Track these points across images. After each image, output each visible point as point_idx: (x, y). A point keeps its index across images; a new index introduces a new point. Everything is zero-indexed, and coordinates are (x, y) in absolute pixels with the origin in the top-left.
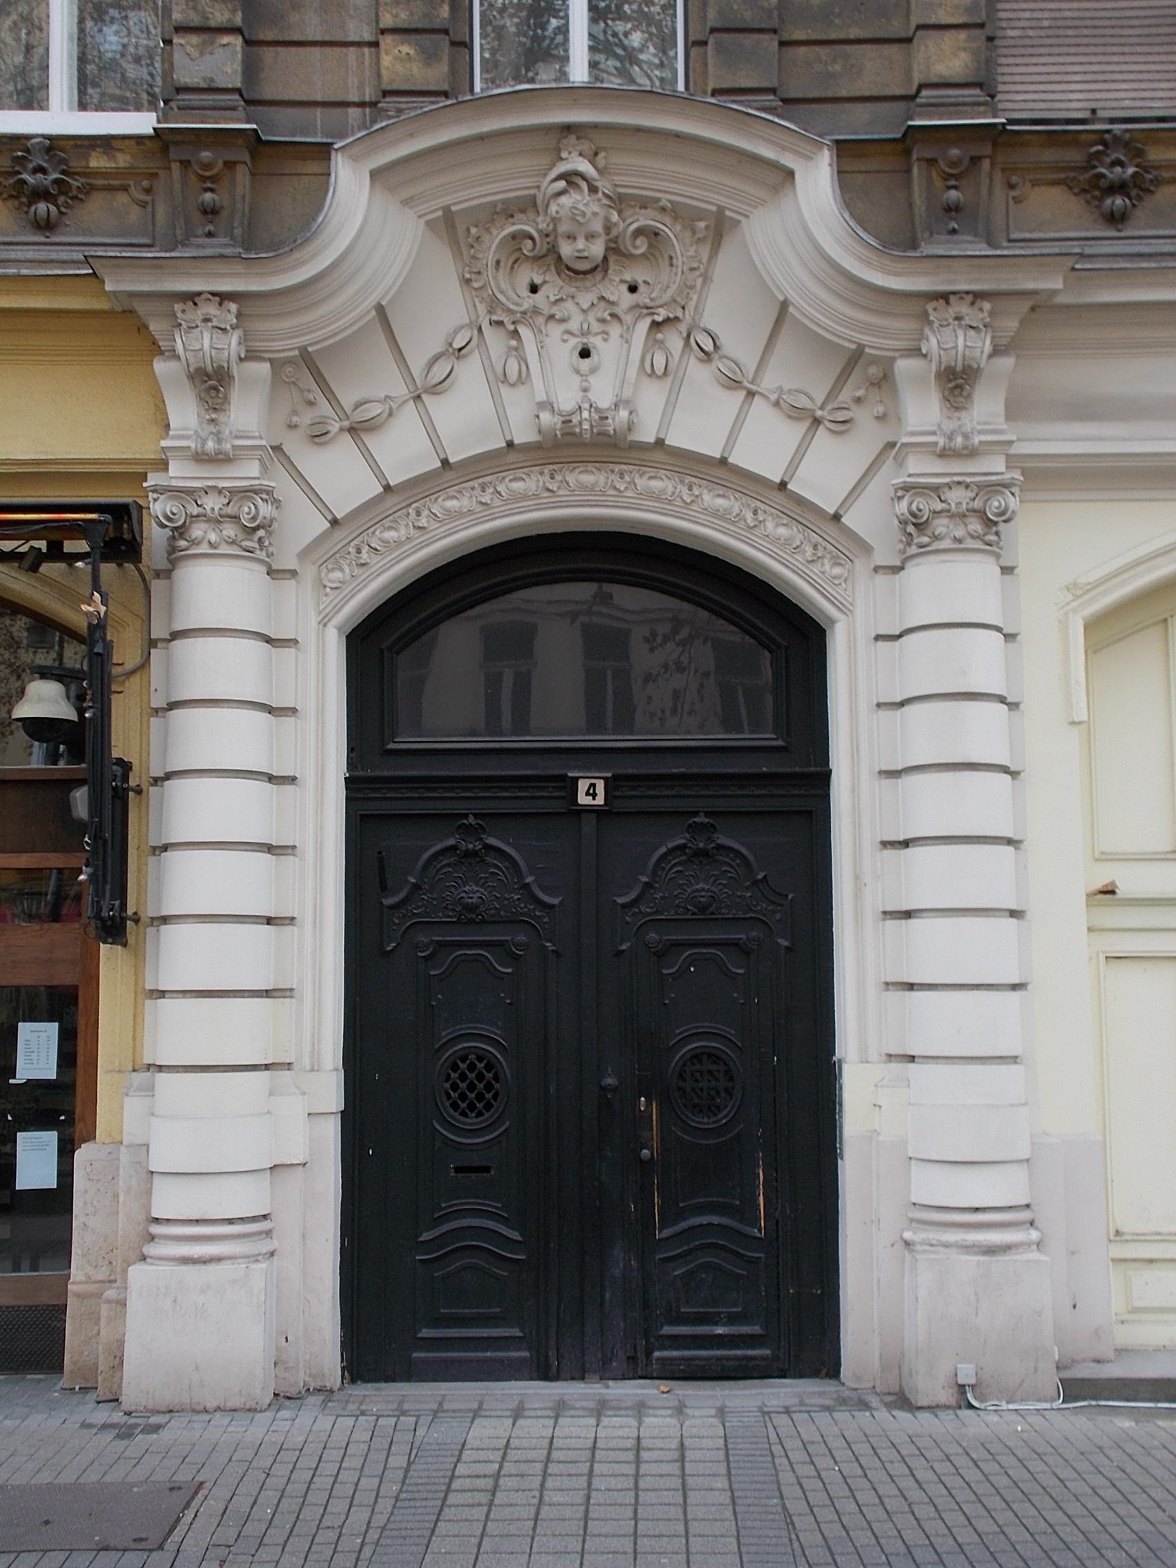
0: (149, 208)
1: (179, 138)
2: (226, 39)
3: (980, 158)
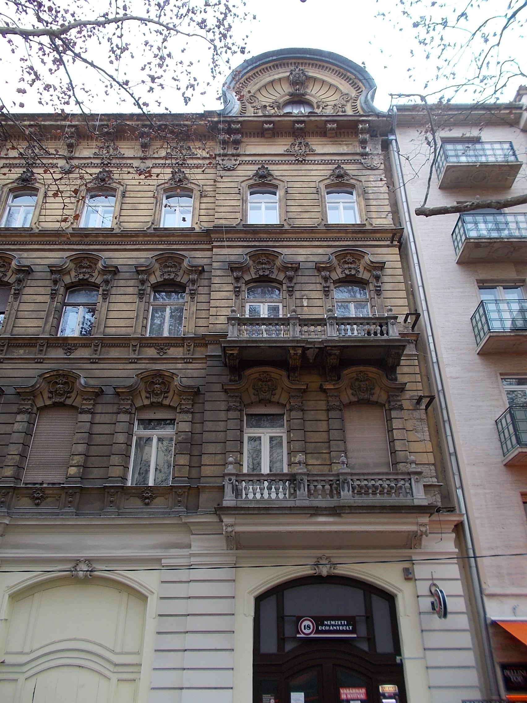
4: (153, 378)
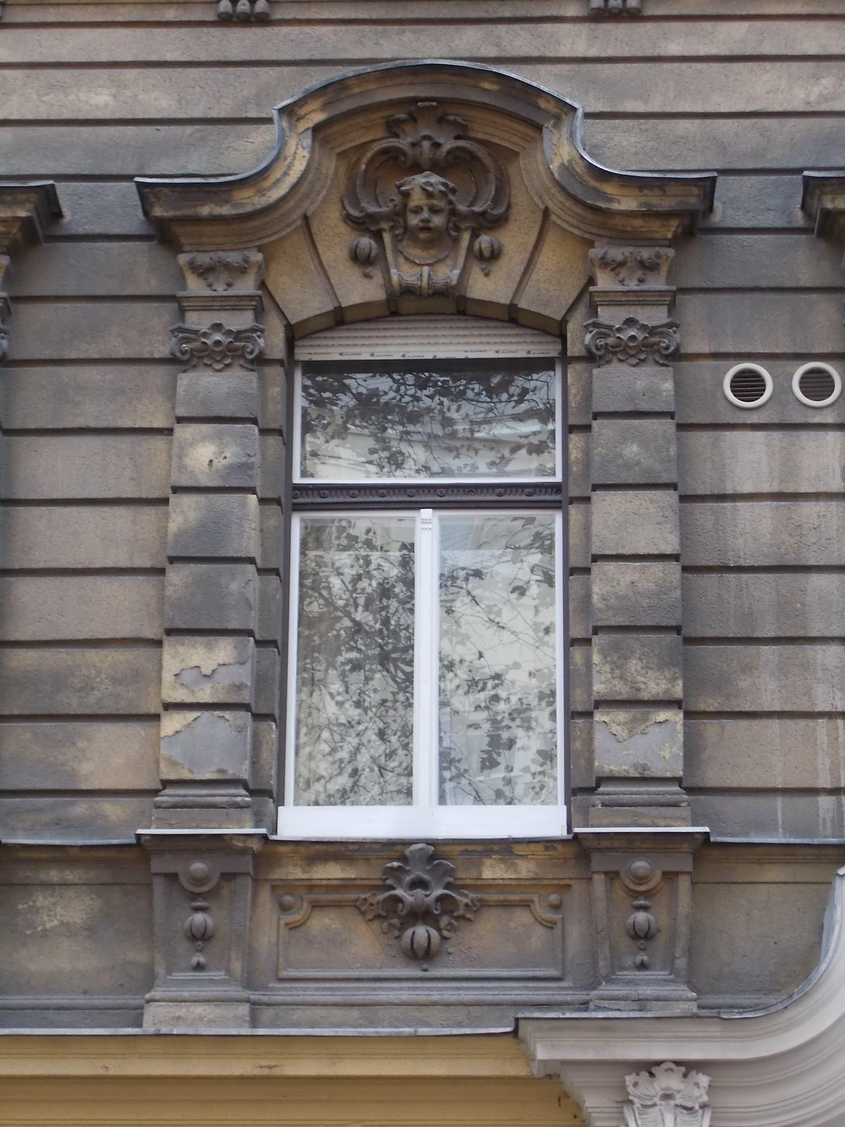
0: (558, 930)
1: (605, 843)
2: (663, 715)
3: (677, 874)
4: (393, 128)
